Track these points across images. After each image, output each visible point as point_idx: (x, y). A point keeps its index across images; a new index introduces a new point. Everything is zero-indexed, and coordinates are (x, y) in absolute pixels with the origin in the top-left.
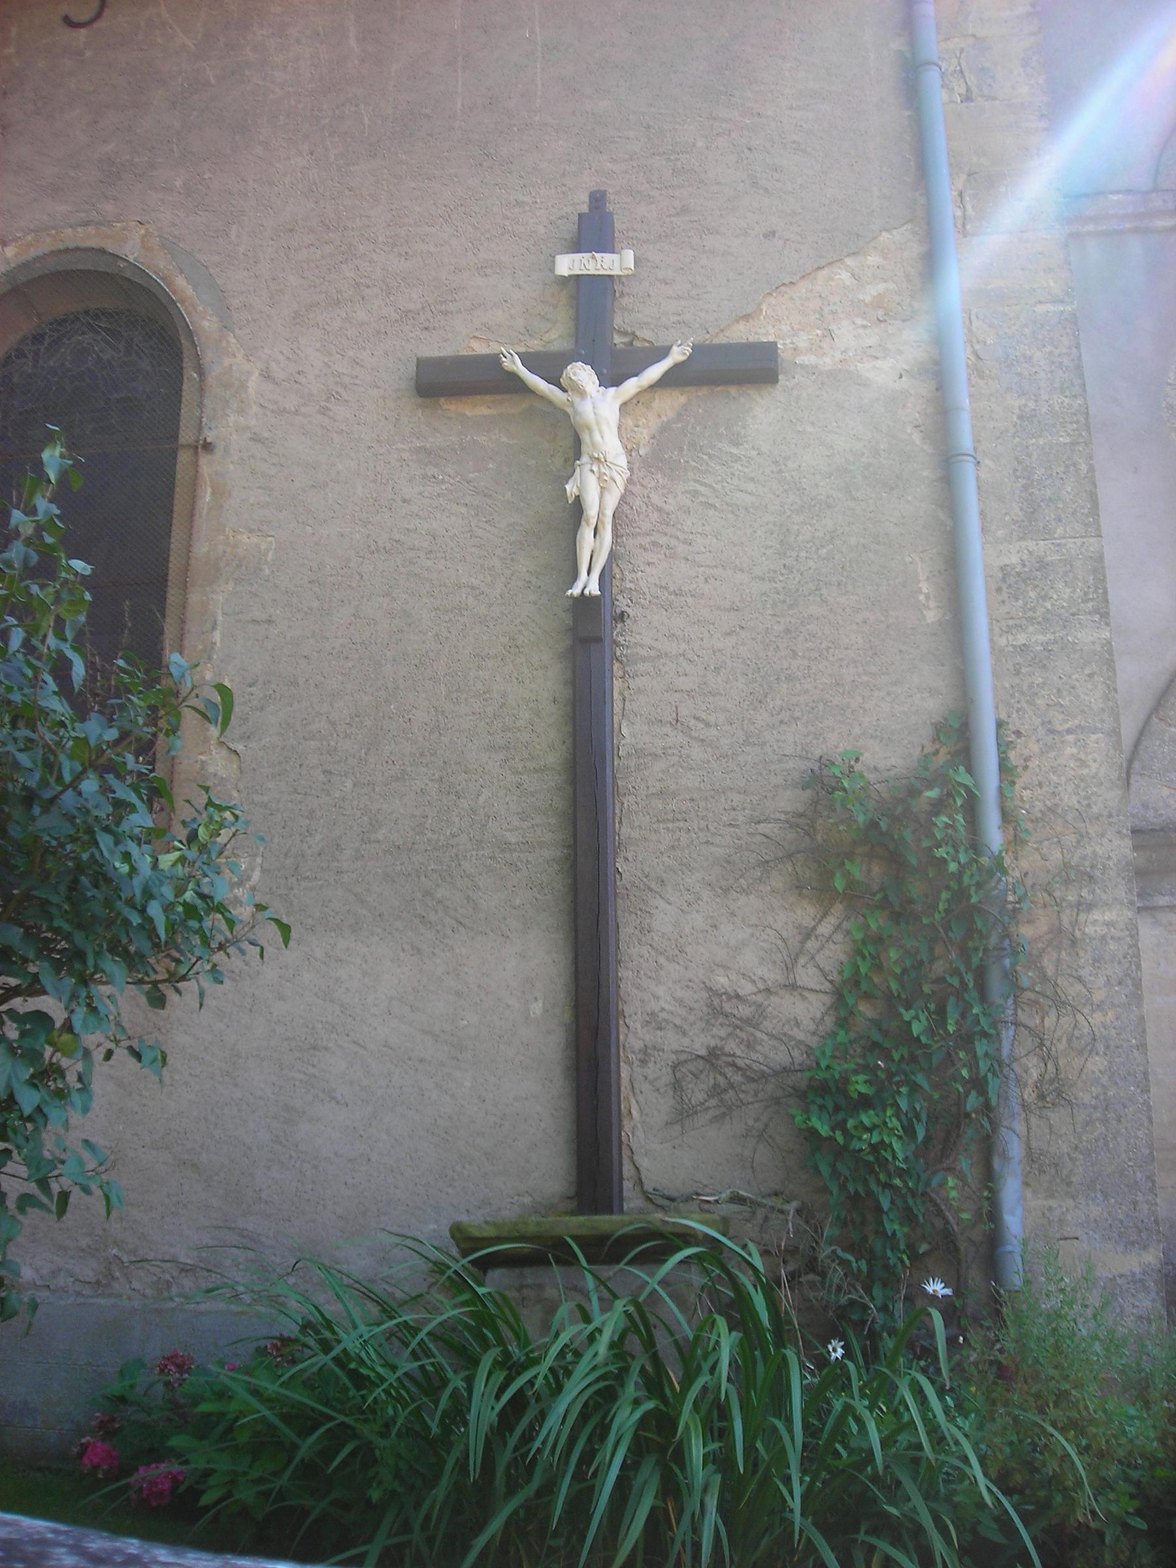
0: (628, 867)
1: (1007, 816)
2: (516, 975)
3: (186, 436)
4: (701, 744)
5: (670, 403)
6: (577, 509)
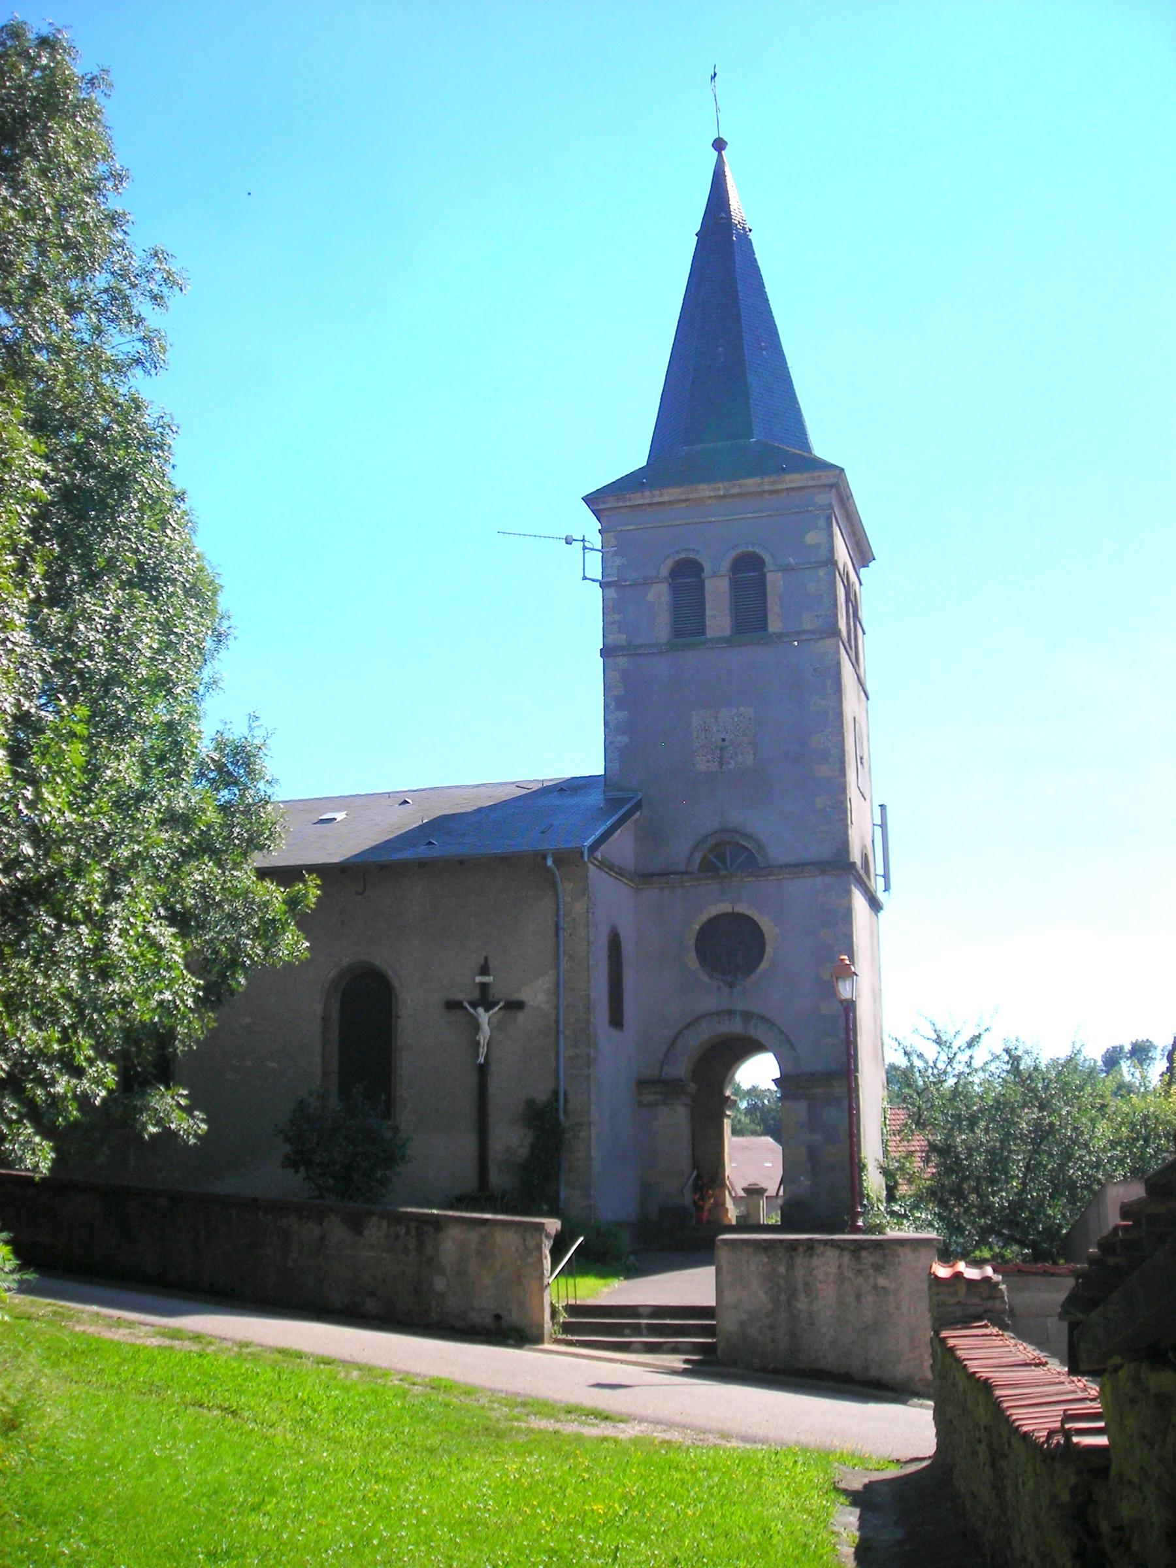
0: (492, 1120)
1: (565, 1113)
2: (467, 1143)
3: (394, 1014)
4: (507, 1093)
5: (502, 1012)
6: (478, 1043)
